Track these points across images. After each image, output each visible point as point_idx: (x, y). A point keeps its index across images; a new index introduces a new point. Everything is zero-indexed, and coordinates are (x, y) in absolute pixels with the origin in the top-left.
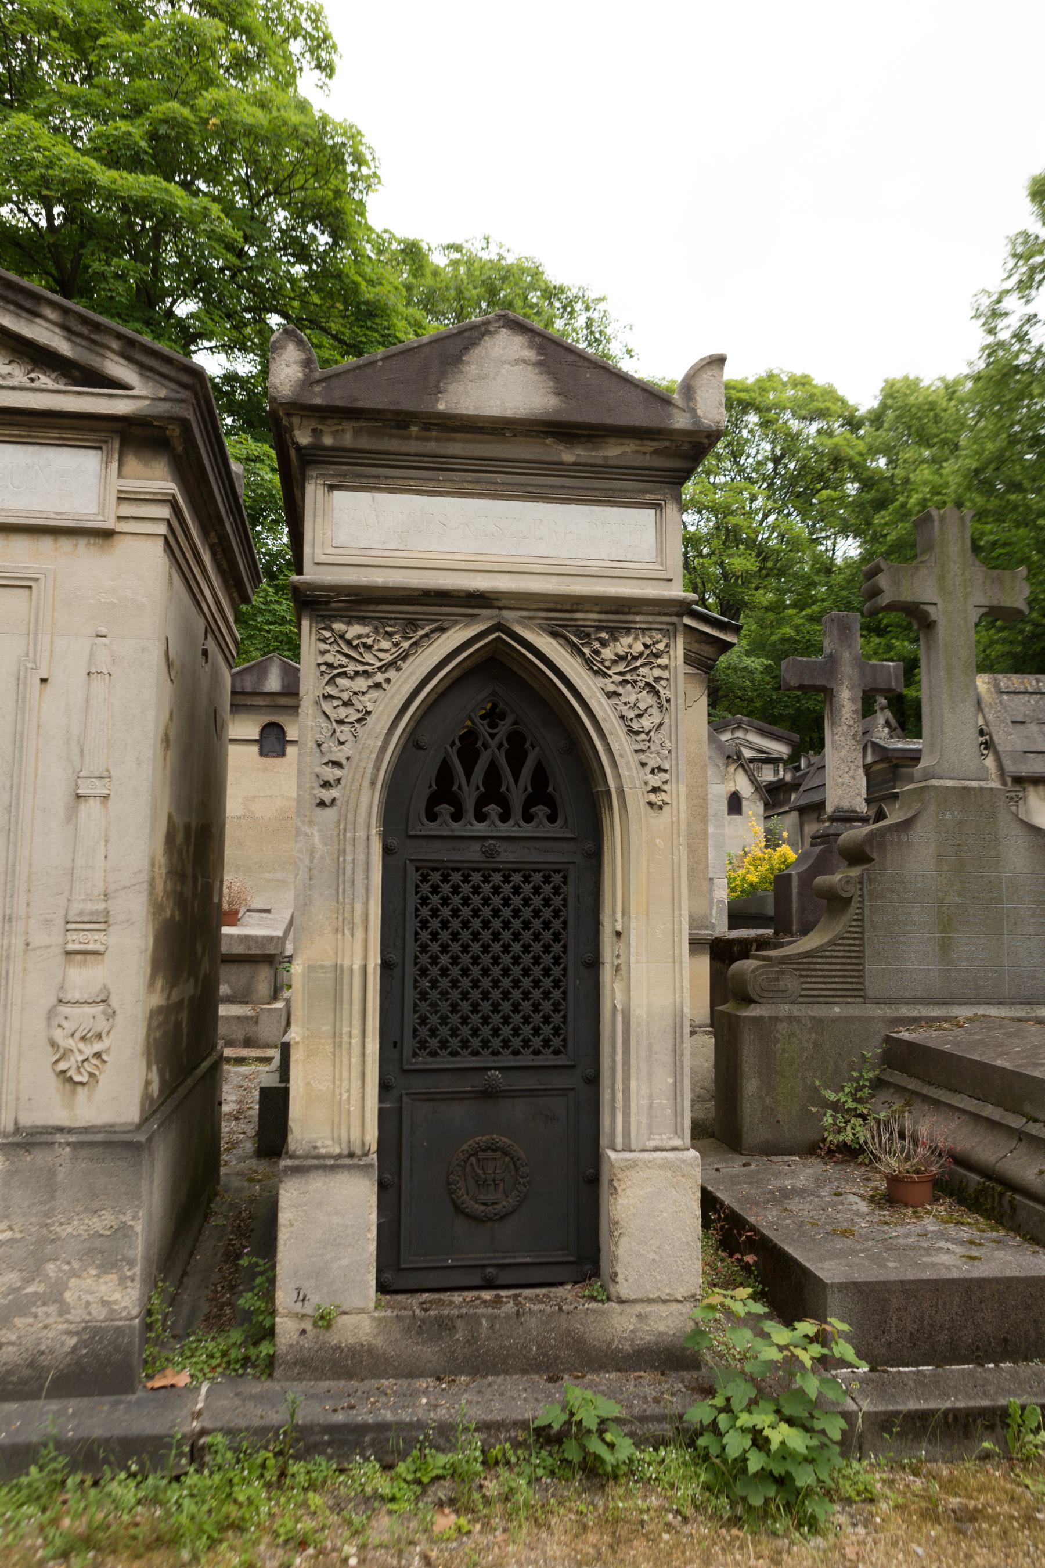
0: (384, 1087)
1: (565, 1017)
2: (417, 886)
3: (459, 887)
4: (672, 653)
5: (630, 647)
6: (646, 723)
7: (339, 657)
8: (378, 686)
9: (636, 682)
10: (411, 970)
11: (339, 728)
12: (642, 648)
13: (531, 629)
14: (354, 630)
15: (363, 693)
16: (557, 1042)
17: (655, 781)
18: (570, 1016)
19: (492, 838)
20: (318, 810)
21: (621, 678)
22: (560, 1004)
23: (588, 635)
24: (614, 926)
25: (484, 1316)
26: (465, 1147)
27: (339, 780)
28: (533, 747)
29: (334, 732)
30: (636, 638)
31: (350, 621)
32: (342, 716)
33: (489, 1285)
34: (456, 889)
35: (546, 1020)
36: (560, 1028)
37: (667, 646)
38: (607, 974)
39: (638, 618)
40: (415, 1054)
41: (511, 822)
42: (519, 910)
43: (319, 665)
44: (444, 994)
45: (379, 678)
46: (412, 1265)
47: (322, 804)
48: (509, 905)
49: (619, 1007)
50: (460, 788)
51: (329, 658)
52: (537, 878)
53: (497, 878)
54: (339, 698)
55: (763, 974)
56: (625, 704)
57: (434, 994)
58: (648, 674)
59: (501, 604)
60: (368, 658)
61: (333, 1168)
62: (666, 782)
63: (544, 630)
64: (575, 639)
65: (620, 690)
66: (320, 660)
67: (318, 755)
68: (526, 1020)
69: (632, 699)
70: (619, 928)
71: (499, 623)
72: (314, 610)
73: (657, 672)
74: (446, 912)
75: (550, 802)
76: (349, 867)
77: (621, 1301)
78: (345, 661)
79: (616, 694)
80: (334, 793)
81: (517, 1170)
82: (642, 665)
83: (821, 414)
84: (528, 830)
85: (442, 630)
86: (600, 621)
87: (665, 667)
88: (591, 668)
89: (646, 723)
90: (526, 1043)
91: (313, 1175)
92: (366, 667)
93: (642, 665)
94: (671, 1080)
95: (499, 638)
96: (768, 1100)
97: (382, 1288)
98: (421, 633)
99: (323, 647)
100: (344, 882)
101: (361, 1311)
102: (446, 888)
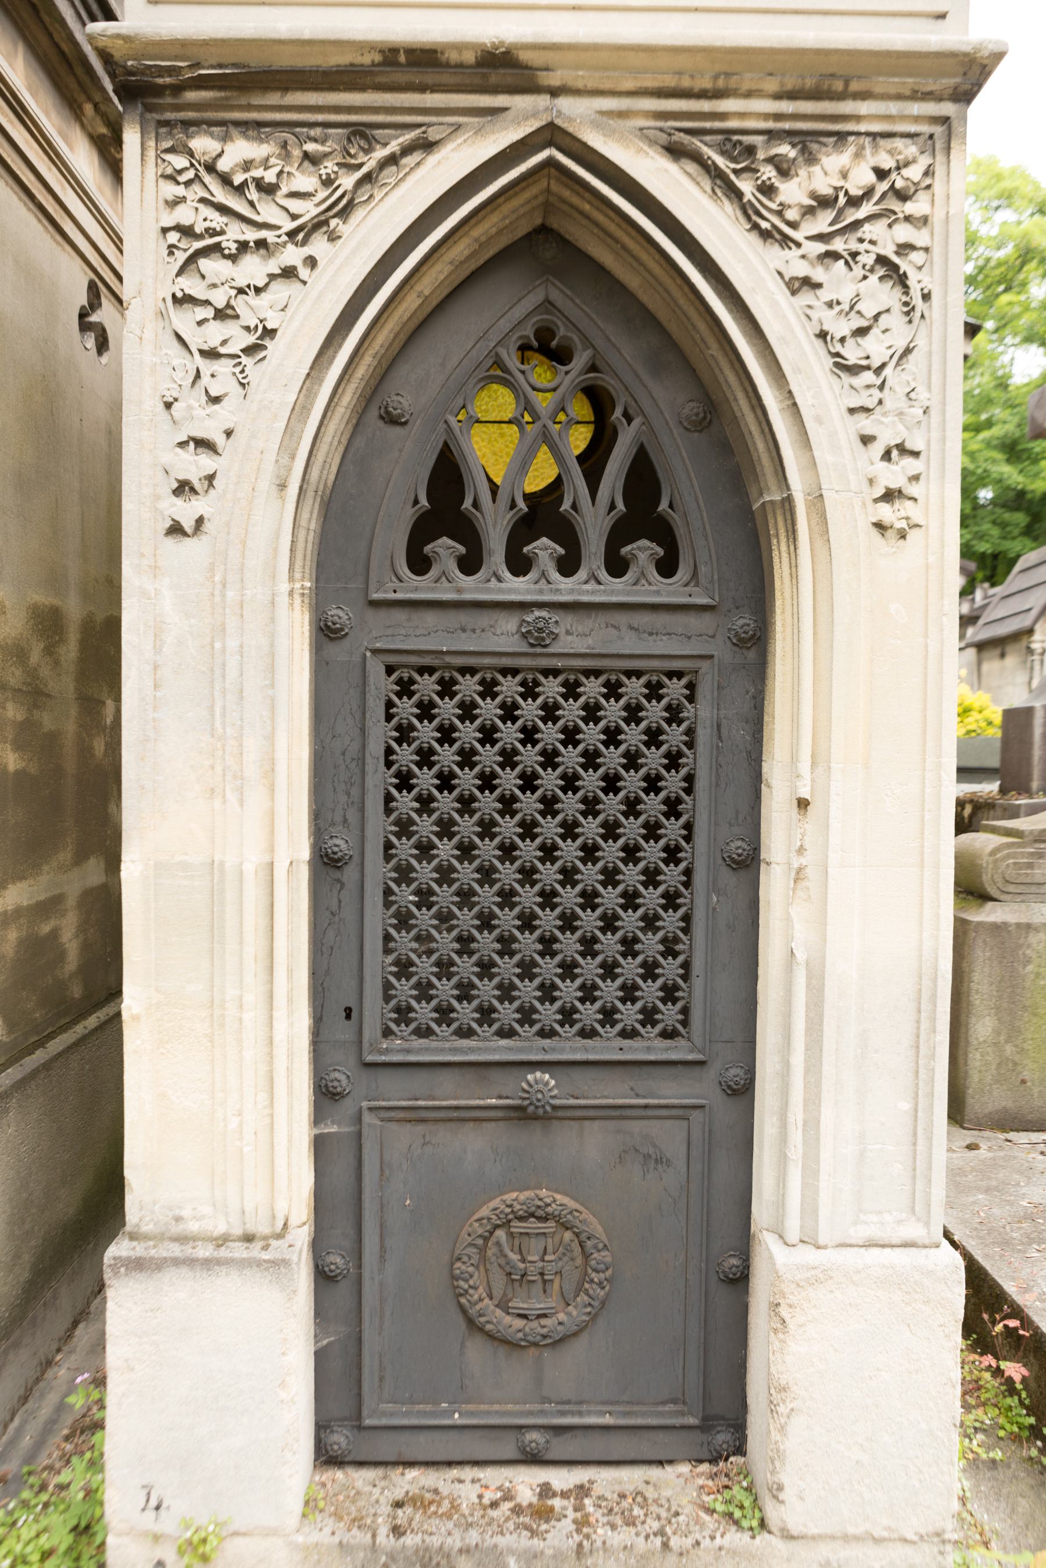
0: (326, 1095)
1: (686, 965)
2: (390, 704)
3: (474, 705)
4: (938, 187)
5: (844, 175)
6: (876, 348)
8: (289, 273)
9: (854, 255)
10: (377, 871)
11: (207, 367)
12: (872, 178)
14: (238, 151)
15: (258, 290)
16: (670, 1014)
17: (893, 475)
18: (698, 967)
19: (541, 605)
20: (170, 542)
21: (821, 248)
22: (676, 940)
23: (750, 151)
24: (794, 788)
25: (512, 1552)
26: (484, 1212)
27: (211, 478)
28: (629, 420)
29: (198, 375)
30: (858, 155)
31: (226, 129)
32: (214, 342)
33: (533, 1459)
34: (468, 711)
35: (650, 970)
36: (676, 988)
38: (774, 885)
39: (864, 108)
40: (387, 1033)
41: (582, 574)
42: (597, 754)
43: (165, 231)
44: (445, 918)
45: (292, 255)
46: (384, 1422)
47: (176, 529)
48: (576, 744)
49: (800, 955)
50: (476, 504)
51: (184, 215)
52: (634, 688)
53: (552, 688)
54: (207, 303)
55: (1008, 856)
56: (830, 305)
57: (425, 919)
58: (884, 238)
59: (554, 79)
60: (268, 212)
61: (208, 1264)
62: (916, 478)
63: (652, 142)
64: (721, 161)
65: (818, 274)
66: (168, 221)
67: (167, 425)
68: (609, 970)
69: (846, 295)
70: (805, 793)
71: (551, 126)
72: (149, 108)
73: (904, 233)
74: (447, 756)
75: (665, 535)
76: (232, 662)
77: (788, 1536)
78: (218, 221)
79: (808, 284)
81: (586, 1256)
83: (1007, 198)
84: (616, 589)
85: (428, 146)
86: (778, 117)
87: (925, 220)
88: (755, 227)
90: (608, 1015)
91: (170, 1275)
92: (263, 234)
94: (906, 1106)
95: (550, 162)
96: (1009, 1049)
97: (327, 1457)
98: (381, 153)
100: (224, 692)
101: (269, 1532)
102: (447, 709)
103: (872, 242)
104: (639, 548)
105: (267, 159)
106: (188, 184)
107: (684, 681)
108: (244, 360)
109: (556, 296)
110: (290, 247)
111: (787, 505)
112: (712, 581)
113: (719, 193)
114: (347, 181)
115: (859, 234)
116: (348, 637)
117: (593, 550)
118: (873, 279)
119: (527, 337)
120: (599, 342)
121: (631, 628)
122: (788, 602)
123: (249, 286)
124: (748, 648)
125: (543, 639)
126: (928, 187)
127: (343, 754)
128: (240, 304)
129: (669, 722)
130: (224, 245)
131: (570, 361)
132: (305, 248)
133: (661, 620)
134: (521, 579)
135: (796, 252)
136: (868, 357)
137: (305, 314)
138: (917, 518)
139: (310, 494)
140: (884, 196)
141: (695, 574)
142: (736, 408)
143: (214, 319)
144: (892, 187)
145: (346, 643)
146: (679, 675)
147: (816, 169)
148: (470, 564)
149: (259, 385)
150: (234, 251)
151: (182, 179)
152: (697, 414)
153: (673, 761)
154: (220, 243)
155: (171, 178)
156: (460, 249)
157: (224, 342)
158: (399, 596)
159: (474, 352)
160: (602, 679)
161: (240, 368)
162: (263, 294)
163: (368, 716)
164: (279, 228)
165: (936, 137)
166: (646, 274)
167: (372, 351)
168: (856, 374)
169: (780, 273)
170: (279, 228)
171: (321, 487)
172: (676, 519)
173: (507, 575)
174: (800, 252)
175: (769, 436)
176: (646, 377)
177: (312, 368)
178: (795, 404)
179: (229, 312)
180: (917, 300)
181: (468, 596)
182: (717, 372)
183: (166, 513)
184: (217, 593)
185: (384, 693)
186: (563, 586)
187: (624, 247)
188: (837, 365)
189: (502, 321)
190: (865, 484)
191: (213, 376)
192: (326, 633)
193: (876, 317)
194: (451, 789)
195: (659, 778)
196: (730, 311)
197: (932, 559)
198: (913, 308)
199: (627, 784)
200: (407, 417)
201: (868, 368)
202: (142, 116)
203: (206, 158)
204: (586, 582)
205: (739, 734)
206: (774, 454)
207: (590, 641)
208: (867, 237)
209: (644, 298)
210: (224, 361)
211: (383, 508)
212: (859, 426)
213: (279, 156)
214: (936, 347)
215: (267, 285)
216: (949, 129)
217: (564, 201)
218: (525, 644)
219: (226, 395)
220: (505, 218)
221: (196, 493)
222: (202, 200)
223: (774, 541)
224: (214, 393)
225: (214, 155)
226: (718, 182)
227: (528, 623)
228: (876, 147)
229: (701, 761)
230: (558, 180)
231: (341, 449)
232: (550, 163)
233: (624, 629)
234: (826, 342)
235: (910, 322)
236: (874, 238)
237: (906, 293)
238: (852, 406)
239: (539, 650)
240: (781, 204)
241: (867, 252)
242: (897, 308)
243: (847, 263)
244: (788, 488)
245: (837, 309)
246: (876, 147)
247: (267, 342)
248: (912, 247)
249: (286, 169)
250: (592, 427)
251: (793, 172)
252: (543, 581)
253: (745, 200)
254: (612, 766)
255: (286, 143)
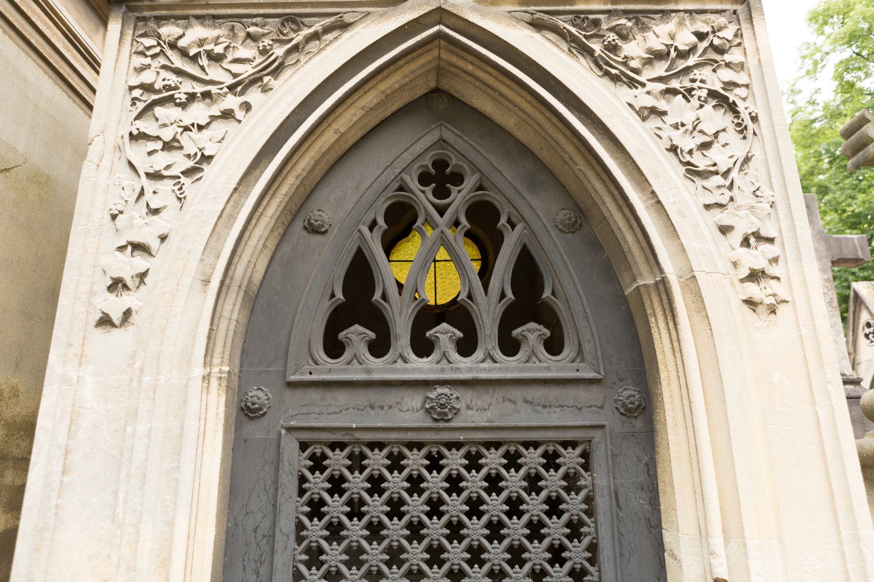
2: (303, 479)
5: (673, 38)
6: (719, 156)
7: (164, 74)
8: (227, 115)
9: (690, 91)
12: (694, 39)
13: (495, 17)
14: (194, 34)
15: (200, 128)
20: (100, 331)
21: (662, 86)
28: (513, 226)
29: (142, 193)
30: (681, 24)
37: (738, 34)
41: (479, 354)
43: (131, 88)
47: (105, 321)
50: (384, 297)
51: (147, 77)
52: (533, 459)
53: (455, 461)
54: (158, 138)
56: (676, 127)
58: (714, 80)
62: (775, 260)
65: (662, 105)
66: (135, 82)
72: (131, 9)
73: (726, 75)
78: (173, 79)
80: (126, 300)
82: (697, 66)
84: (510, 367)
85: (345, 26)
87: (741, 66)
88: (607, 74)
89: (719, 156)
93: (697, 66)
98: (306, 32)
99: (139, 61)
103: (702, 81)
104: (528, 330)
105: (218, 38)
106: (154, 56)
107: (579, 450)
108: (183, 179)
109: (448, 136)
110: (230, 96)
111: (661, 287)
112: (596, 357)
113: (575, 53)
114: (279, 51)
115: (692, 76)
116: (267, 415)
117: (488, 333)
118: (708, 107)
119: (426, 166)
120: (485, 168)
121: (527, 402)
122: (673, 374)
123: (193, 125)
124: (636, 417)
125: (446, 414)
126: (739, 44)
127: (255, 531)
128: (184, 139)
129: (568, 490)
130: (176, 96)
131: (462, 182)
132: (242, 97)
133: (553, 393)
134: (425, 360)
135: (640, 90)
136: (715, 165)
137: (235, 147)
138: (783, 295)
139: (234, 288)
140: (705, 51)
141: (580, 352)
142: (604, 210)
143: (162, 150)
144: (711, 45)
145: (264, 421)
146: (573, 444)
147: (650, 34)
148: (379, 348)
149: (193, 199)
150: (184, 100)
151: (149, 53)
152: (570, 219)
153: (575, 530)
154: (173, 95)
155: (142, 54)
156: (370, 99)
157: (168, 167)
158: (315, 377)
159: (383, 177)
160: (502, 450)
161: (179, 186)
162: (204, 131)
163: (280, 492)
164: (223, 83)
165: (738, 11)
166: (520, 113)
167: (294, 174)
168: (707, 178)
169: (630, 105)
170: (223, 83)
171: (245, 283)
172: (559, 305)
173: (412, 356)
174: (646, 90)
175: (638, 230)
176: (525, 193)
177: (239, 184)
178: (659, 202)
179: (176, 144)
180: (748, 121)
181: (376, 376)
182: (585, 182)
183: (98, 307)
184: (135, 378)
185: (296, 467)
186: (462, 365)
187: (501, 95)
188: (688, 171)
189: (405, 154)
190: (730, 266)
191: (155, 192)
192: (245, 413)
193: (716, 135)
194: (360, 564)
195: (563, 548)
196: (593, 134)
197: (804, 331)
198: (746, 127)
199: (532, 556)
200: (327, 227)
201: (717, 173)
202: (124, 13)
203: (170, 38)
204: (483, 361)
205: (638, 502)
206: (644, 244)
207: (489, 414)
208: (698, 77)
209: (519, 134)
210: (166, 182)
211: (303, 301)
212: (716, 219)
213: (227, 37)
214: (770, 156)
215: (208, 124)
216: (749, 6)
217: (452, 64)
218: (430, 420)
219: (164, 207)
220: (405, 77)
221: (128, 289)
222: (164, 67)
223: (652, 320)
224: (153, 206)
225: (176, 36)
226: (573, 45)
227: (432, 399)
228: (693, 20)
229: (602, 528)
230: (446, 49)
231: (268, 253)
232: (439, 35)
233: (520, 403)
234: (677, 154)
235: (745, 138)
236: (704, 78)
237: (738, 117)
238: (707, 203)
239: (442, 424)
240: (626, 57)
241: (700, 88)
242: (731, 128)
243: (684, 97)
244: (661, 271)
245: (682, 129)
246: (693, 20)
247: (204, 166)
248: (736, 85)
249: (232, 45)
250: (480, 262)
251: (631, 37)
252: (445, 361)
253: (596, 55)
254: (516, 537)
255: (233, 26)
